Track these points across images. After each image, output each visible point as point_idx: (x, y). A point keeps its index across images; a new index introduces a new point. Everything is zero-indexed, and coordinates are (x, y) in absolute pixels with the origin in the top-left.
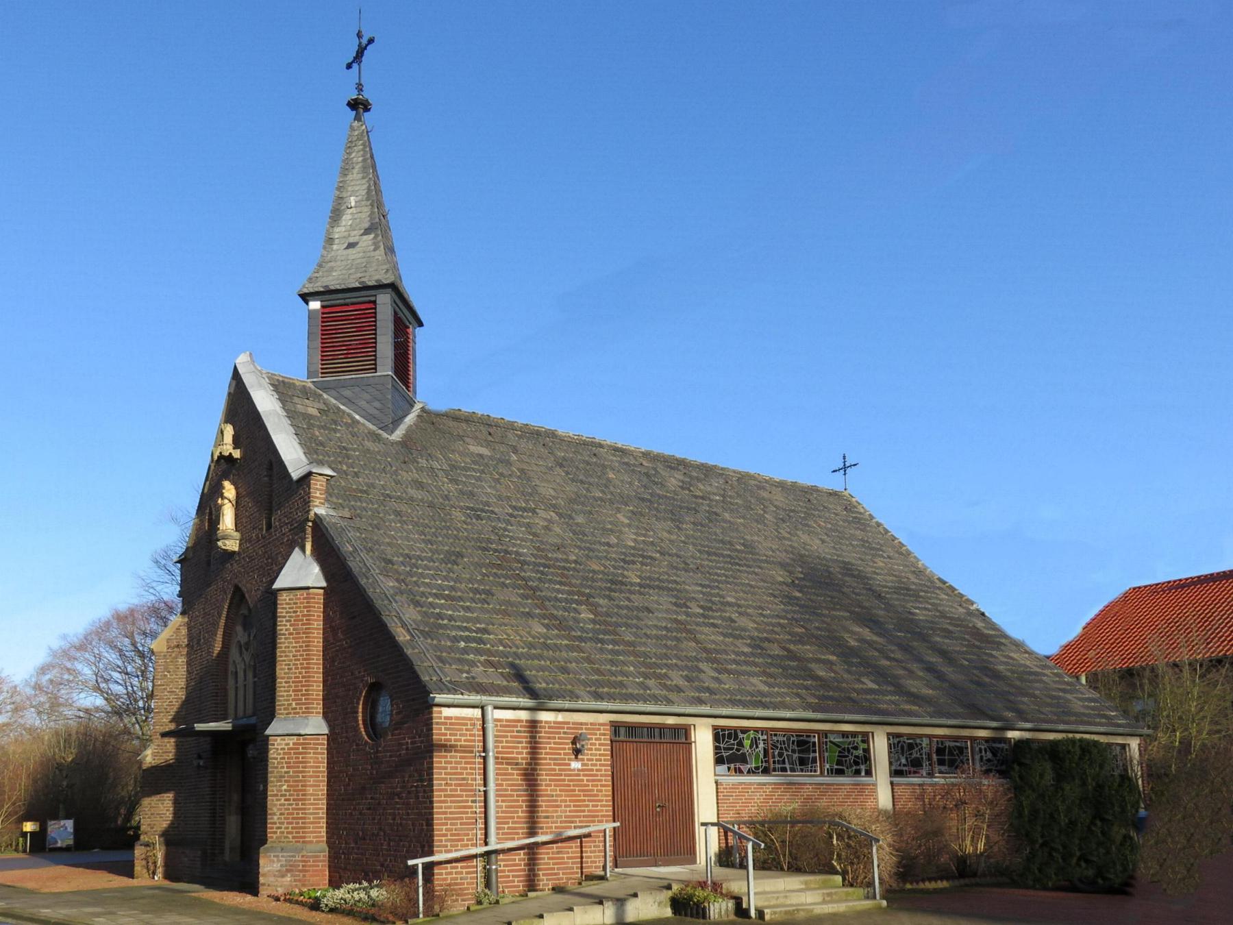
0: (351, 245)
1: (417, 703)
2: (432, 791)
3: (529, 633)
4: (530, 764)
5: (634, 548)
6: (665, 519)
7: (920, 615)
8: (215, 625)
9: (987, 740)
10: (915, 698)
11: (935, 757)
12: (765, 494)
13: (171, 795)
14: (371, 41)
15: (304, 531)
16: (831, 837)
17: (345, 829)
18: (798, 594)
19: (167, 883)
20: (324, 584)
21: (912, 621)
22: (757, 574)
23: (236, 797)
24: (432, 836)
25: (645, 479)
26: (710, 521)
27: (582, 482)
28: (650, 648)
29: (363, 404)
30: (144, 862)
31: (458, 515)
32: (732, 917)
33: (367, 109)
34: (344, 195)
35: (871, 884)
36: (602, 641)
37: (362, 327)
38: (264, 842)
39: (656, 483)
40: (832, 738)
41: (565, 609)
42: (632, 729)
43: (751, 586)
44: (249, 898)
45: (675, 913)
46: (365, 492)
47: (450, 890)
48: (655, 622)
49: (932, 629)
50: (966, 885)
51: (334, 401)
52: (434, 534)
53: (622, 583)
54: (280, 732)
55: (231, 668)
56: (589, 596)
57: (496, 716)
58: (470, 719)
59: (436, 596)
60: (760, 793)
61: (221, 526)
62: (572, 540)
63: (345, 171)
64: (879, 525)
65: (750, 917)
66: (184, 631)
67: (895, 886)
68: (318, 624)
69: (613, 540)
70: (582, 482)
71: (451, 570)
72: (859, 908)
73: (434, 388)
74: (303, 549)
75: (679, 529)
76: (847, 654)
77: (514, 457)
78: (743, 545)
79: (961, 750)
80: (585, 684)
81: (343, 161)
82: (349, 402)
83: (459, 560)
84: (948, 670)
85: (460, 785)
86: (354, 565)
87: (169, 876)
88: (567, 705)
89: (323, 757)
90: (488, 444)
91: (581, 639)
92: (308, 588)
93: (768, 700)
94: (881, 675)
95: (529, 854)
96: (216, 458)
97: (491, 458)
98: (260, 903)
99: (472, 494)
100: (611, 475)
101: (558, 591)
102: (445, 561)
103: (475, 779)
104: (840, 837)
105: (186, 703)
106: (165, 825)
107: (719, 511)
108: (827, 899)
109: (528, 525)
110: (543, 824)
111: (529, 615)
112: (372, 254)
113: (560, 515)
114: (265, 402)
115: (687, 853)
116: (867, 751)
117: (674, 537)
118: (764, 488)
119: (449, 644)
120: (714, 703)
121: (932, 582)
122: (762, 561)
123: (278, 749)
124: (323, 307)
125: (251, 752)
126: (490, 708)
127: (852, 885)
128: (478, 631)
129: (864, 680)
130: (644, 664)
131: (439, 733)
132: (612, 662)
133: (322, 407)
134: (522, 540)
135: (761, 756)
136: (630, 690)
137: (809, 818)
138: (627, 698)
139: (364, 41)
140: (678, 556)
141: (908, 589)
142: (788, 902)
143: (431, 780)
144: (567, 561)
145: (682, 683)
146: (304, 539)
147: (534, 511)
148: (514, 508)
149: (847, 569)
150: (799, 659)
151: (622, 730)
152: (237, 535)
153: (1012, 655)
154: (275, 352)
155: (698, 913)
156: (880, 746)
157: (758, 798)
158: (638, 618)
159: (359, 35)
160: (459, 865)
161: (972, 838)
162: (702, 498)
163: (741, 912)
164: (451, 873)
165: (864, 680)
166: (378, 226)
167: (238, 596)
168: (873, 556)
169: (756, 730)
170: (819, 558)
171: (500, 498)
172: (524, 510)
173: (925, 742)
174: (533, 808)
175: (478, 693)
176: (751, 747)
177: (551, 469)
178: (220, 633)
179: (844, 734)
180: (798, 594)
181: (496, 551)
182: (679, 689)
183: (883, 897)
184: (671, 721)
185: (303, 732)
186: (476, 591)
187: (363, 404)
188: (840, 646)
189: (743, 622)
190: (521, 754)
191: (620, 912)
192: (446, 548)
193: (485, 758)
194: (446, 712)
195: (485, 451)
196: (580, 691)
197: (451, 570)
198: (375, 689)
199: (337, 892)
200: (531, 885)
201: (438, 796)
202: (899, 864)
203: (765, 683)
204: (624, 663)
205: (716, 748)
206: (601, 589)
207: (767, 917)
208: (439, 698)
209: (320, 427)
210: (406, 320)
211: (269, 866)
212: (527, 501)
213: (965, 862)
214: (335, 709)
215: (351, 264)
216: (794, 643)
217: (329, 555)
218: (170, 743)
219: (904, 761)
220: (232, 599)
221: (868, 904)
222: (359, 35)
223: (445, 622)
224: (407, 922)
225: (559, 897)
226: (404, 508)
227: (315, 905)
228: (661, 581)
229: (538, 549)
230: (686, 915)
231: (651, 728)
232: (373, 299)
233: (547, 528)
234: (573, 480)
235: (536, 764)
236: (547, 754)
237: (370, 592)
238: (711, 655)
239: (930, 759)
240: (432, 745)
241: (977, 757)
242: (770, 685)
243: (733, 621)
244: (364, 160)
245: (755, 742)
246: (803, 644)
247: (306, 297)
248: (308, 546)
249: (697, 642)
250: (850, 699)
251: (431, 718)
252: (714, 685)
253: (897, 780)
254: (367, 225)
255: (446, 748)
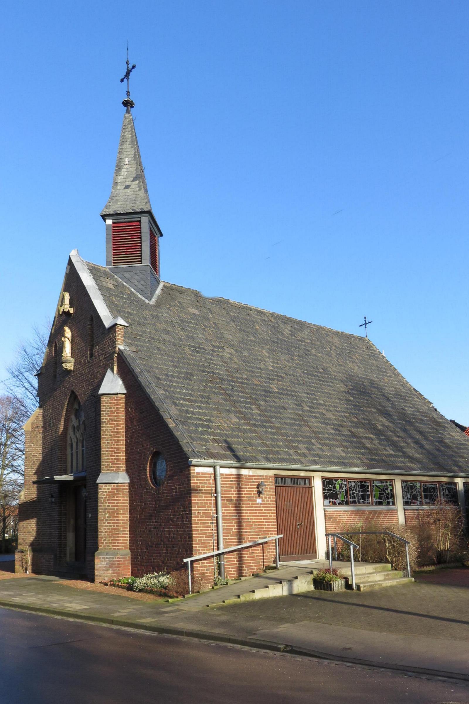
0: (127, 187)
1: (182, 464)
2: (191, 517)
3: (230, 422)
4: (237, 500)
5: (272, 371)
6: (285, 354)
7: (409, 411)
8: (60, 415)
9: (446, 483)
10: (412, 459)
11: (423, 494)
12: (330, 339)
13: (34, 521)
14: (134, 67)
15: (113, 359)
16: (385, 541)
17: (140, 541)
18: (352, 399)
19: (34, 575)
20: (125, 392)
21: (404, 414)
22: (331, 387)
23: (72, 522)
24: (192, 544)
25: (273, 329)
26: (306, 355)
27: (244, 331)
28: (287, 430)
29: (135, 282)
30: (20, 563)
31: (187, 350)
32: (344, 590)
33: (132, 107)
34: (122, 157)
35: (405, 569)
36: (265, 427)
37: (132, 235)
38: (97, 549)
39: (279, 332)
40: (376, 483)
41: (246, 408)
42: (284, 479)
43: (330, 394)
44: (89, 584)
45: (315, 588)
46: (141, 336)
47: (203, 576)
48: (288, 416)
49: (414, 418)
50: (443, 568)
51: (120, 280)
52: (178, 362)
53: (270, 392)
54: (104, 482)
55: (69, 442)
56: (256, 400)
57: (221, 472)
58: (208, 474)
59: (184, 399)
60: (346, 515)
61: (64, 354)
62: (244, 366)
63: (122, 143)
64: (383, 357)
65: (353, 589)
66: (41, 418)
67: (417, 569)
68: (122, 416)
69: (263, 366)
70: (244, 331)
71: (188, 384)
72: (402, 583)
73: (170, 273)
74: (112, 370)
75: (293, 359)
76: (379, 433)
77: (211, 316)
78: (323, 369)
79: (434, 489)
80: (261, 452)
81: (121, 137)
82: (128, 281)
83: (191, 378)
84: (424, 442)
85: (205, 513)
86: (142, 379)
87: (34, 571)
88: (255, 465)
89: (127, 497)
90: (197, 308)
91: (255, 425)
92: (117, 394)
93: (346, 461)
94: (395, 446)
95: (238, 554)
96: (61, 313)
97: (199, 315)
98: (96, 586)
99: (193, 338)
100: (257, 327)
101: (241, 397)
102: (185, 378)
103: (212, 510)
104: (390, 542)
105: (42, 463)
106: (31, 539)
107: (310, 349)
108: (387, 577)
109: (221, 357)
110: (245, 536)
111: (229, 411)
112: (138, 193)
113: (236, 351)
114: (87, 280)
115: (310, 551)
116: (392, 490)
117: (290, 364)
118: (328, 335)
119: (194, 428)
120: (323, 463)
121: (411, 391)
122: (332, 379)
123: (104, 491)
124: (113, 223)
125: (84, 493)
126: (218, 467)
127: (396, 569)
128: (207, 421)
129: (388, 449)
130: (287, 441)
131: (195, 482)
132: (272, 440)
133: (115, 283)
134: (220, 365)
135: (344, 494)
136: (282, 456)
137: (369, 531)
138: (282, 460)
139: (130, 67)
140: (294, 376)
141: (401, 396)
142: (369, 580)
143: (191, 510)
144: (242, 378)
145: (306, 451)
146: (113, 364)
147: (223, 348)
148: (214, 346)
149: (372, 383)
150: (356, 436)
151: (280, 480)
152: (72, 360)
153: (451, 433)
154: (91, 251)
155: (327, 588)
156: (398, 487)
157: (344, 519)
158: (281, 413)
159: (127, 63)
160: (205, 561)
161: (444, 541)
162: (301, 341)
163: (349, 586)
164: (201, 567)
165: (388, 449)
166: (139, 177)
167: (74, 396)
168: (383, 375)
169: (342, 479)
170: (358, 377)
171: (206, 340)
172: (219, 347)
173: (418, 484)
174: (240, 527)
175: (212, 458)
176: (340, 489)
177: (228, 323)
178: (63, 419)
179: (382, 481)
180: (352, 399)
181: (208, 372)
182: (304, 455)
183: (412, 577)
184: (302, 474)
185: (117, 482)
186: (202, 397)
187: (135, 282)
188: (374, 429)
189: (329, 415)
190: (233, 495)
191: (290, 588)
192: (185, 370)
193: (216, 497)
194: (198, 470)
195: (196, 312)
196: (259, 456)
197: (188, 384)
198: (156, 455)
199: (142, 579)
200: (240, 574)
201: (194, 520)
202: (419, 557)
203: (343, 451)
204: (277, 440)
205: (324, 490)
206: (261, 395)
207: (362, 589)
208: (195, 461)
209: (116, 296)
210: (156, 231)
211: (101, 564)
212: (219, 342)
213: (440, 555)
214: (133, 467)
215: (126, 200)
216: (353, 427)
217: (127, 374)
218: (34, 489)
219: (409, 496)
220: (69, 399)
221: (406, 580)
222: (127, 63)
223: (190, 415)
224: (184, 597)
225: (257, 580)
226: (161, 346)
227: (130, 587)
228: (288, 390)
229: (228, 371)
230: (321, 589)
231: (293, 478)
232: (139, 219)
233: (231, 359)
234: (240, 330)
235: (241, 500)
236: (245, 494)
237: (152, 397)
238: (317, 435)
239: (421, 495)
240: (190, 490)
241: (442, 493)
242: (346, 453)
243: (324, 415)
244: (132, 137)
245: (341, 487)
246: (358, 427)
247: (104, 217)
248: (115, 368)
249: (309, 427)
250: (384, 461)
251: (190, 474)
252: (320, 453)
253: (407, 507)
254: (134, 175)
255: (198, 491)
